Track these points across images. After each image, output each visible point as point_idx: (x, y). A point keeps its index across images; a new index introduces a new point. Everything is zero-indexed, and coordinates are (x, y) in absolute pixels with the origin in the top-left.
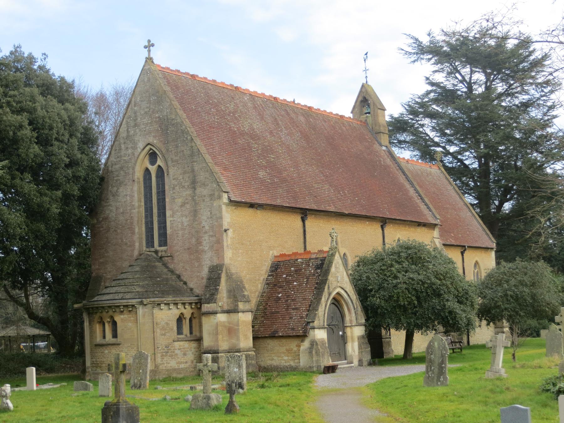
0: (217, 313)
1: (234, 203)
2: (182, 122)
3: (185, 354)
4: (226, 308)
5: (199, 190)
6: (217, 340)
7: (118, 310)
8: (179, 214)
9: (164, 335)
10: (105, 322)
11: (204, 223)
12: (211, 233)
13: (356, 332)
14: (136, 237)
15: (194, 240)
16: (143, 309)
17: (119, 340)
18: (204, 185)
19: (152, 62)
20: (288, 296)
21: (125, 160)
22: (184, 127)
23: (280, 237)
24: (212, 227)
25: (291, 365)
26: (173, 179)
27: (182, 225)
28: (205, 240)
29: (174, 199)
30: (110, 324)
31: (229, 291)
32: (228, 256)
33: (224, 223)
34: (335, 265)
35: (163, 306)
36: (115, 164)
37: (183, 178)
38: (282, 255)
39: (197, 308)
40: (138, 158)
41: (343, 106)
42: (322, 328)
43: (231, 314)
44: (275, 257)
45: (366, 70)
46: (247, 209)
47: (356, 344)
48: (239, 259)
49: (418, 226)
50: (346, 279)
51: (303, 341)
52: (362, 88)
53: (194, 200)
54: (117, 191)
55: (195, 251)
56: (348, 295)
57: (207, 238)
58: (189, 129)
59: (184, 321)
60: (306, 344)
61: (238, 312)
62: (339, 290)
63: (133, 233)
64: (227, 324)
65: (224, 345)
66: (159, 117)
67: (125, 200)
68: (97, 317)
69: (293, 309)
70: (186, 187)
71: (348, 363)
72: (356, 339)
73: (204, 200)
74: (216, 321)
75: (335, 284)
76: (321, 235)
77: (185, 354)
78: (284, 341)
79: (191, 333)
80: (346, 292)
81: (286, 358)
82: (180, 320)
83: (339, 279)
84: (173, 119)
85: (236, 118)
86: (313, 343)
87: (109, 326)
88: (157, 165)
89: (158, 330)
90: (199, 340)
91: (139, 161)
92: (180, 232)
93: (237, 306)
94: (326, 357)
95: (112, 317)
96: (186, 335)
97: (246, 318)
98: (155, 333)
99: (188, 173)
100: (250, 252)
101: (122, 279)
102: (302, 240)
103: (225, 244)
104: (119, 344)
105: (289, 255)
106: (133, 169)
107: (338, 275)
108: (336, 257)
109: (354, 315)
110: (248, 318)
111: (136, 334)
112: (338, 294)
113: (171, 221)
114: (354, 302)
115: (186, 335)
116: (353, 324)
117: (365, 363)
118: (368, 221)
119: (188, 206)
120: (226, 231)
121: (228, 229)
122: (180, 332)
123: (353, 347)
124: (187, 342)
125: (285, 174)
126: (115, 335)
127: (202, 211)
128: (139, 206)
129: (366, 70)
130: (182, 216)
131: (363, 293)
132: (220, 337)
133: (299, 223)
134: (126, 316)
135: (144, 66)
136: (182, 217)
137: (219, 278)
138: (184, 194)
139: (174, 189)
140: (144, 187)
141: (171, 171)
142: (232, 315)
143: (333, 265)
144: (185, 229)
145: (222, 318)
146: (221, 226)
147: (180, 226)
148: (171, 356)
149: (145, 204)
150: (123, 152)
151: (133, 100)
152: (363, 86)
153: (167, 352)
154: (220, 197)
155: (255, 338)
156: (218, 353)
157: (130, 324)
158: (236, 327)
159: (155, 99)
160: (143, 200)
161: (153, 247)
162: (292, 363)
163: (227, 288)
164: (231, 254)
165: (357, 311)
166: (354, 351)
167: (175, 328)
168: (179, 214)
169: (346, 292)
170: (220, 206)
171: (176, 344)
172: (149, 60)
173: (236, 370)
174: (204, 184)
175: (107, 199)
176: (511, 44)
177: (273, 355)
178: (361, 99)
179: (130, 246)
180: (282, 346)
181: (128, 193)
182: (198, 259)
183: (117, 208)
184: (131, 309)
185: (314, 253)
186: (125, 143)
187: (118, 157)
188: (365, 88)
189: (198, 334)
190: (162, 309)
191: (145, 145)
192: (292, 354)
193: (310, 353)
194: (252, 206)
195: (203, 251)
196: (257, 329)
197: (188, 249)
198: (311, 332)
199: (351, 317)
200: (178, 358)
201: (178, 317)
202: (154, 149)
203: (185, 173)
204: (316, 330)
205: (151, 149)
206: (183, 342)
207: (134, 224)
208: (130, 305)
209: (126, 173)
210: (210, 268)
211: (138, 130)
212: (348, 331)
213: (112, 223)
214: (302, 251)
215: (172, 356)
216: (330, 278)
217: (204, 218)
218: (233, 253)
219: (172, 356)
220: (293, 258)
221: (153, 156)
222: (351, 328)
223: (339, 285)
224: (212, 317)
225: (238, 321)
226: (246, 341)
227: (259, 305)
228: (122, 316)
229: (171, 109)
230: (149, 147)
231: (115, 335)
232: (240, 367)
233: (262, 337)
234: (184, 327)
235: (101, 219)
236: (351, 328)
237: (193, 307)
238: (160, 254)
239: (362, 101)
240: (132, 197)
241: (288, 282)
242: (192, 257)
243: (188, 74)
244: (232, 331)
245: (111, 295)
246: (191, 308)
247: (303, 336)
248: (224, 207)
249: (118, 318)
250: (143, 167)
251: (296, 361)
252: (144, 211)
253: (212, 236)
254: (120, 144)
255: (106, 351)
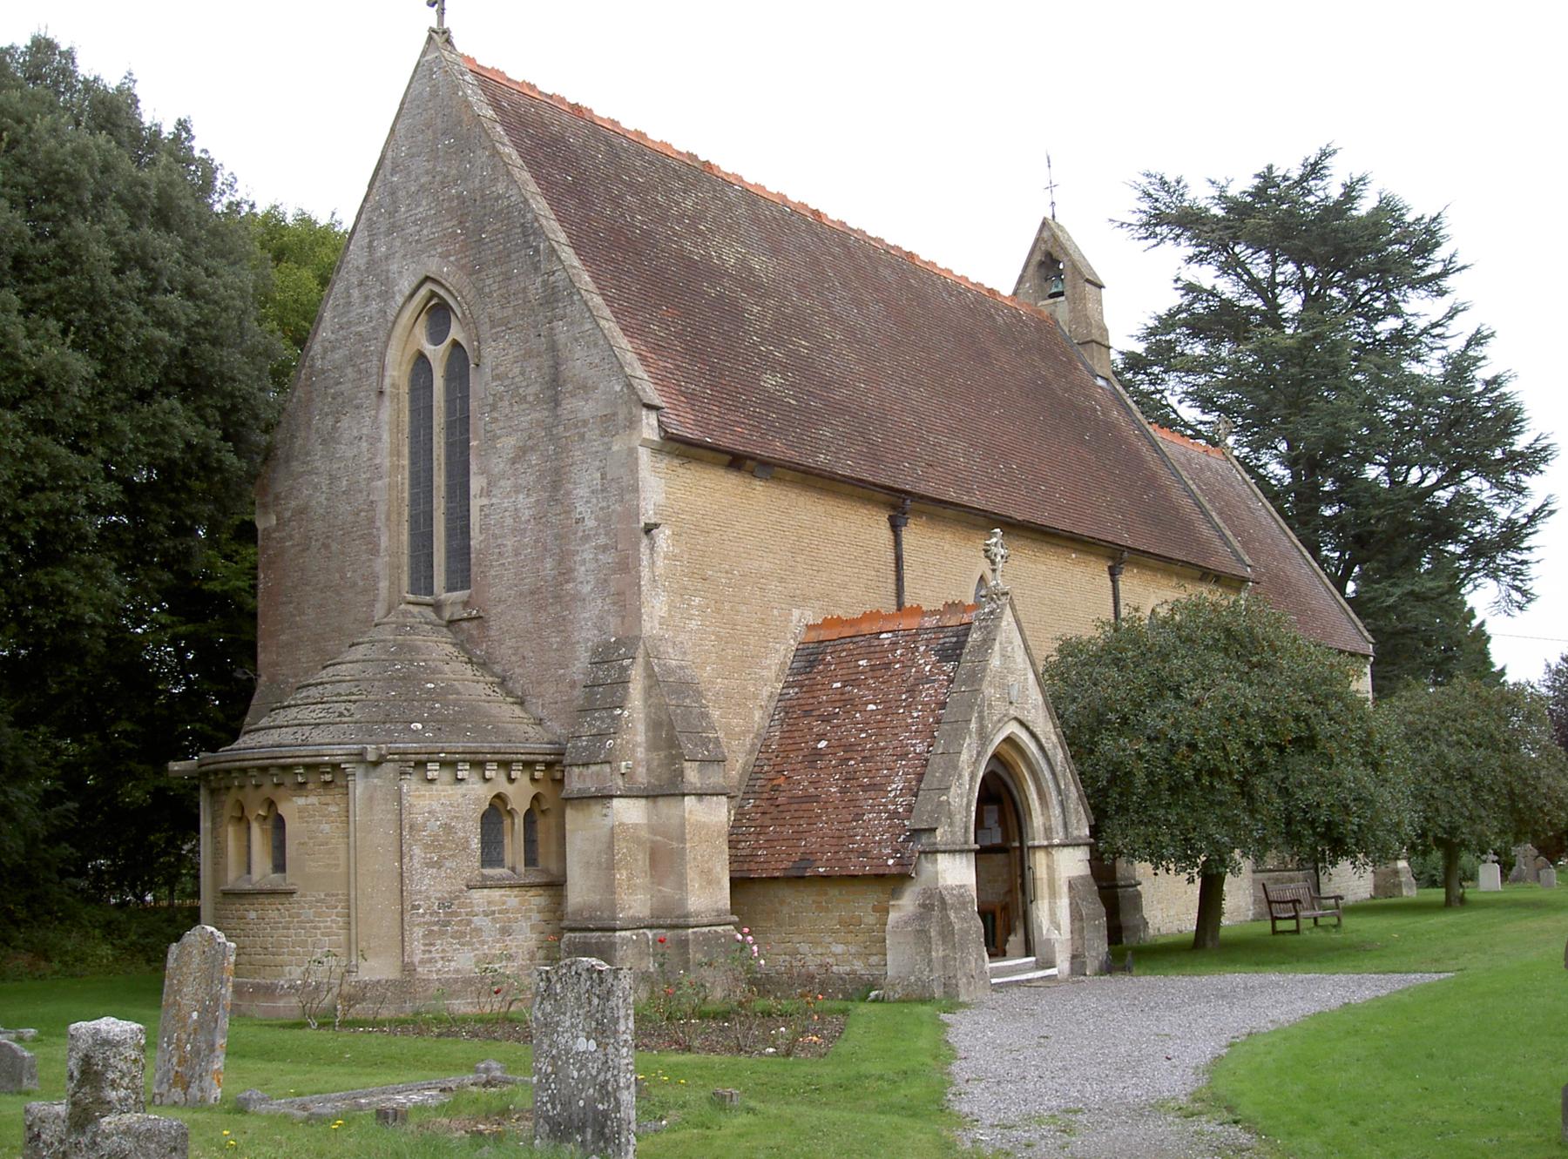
0: (612, 797)
1: (679, 447)
2: (526, 201)
3: (505, 931)
4: (642, 777)
5: (568, 405)
6: (610, 887)
7: (288, 780)
8: (507, 484)
9: (438, 865)
10: (252, 818)
11: (581, 508)
12: (602, 540)
13: (1061, 869)
14: (381, 564)
15: (549, 563)
16: (366, 775)
17: (290, 880)
18: (585, 388)
19: (448, 41)
20: (849, 748)
21: (359, 334)
22: (529, 216)
23: (828, 562)
24: (605, 520)
25: (853, 972)
26: (494, 379)
27: (516, 518)
28: (583, 562)
29: (495, 438)
30: (268, 826)
31: (655, 725)
32: (655, 610)
33: (642, 504)
34: (1003, 649)
35: (433, 770)
36: (334, 349)
37: (522, 374)
38: (828, 623)
39: (554, 780)
40: (394, 323)
41: (997, 268)
42: (961, 851)
43: (661, 802)
44: (809, 627)
45: (1051, 187)
46: (722, 472)
47: (1064, 903)
48: (693, 625)
49: (1201, 579)
50: (1035, 696)
51: (896, 893)
52: (1041, 231)
53: (554, 439)
54: (334, 428)
55: (554, 598)
56: (1041, 748)
57: (588, 556)
58: (544, 222)
59: (507, 822)
60: (907, 903)
61: (684, 795)
62: (1013, 728)
63: (374, 551)
64: (644, 834)
65: (636, 902)
66: (459, 196)
67: (355, 451)
68: (229, 800)
69: (865, 788)
70: (530, 399)
71: (1039, 966)
72: (1065, 889)
73: (582, 437)
74: (608, 822)
75: (999, 708)
76: (945, 568)
77: (505, 931)
78: (834, 892)
79: (530, 860)
80: (1033, 735)
81: (839, 949)
82: (495, 812)
83: (1014, 693)
84: (499, 197)
85: (700, 233)
86: (935, 903)
87: (263, 830)
88: (449, 340)
89: (417, 850)
90: (555, 885)
91: (399, 331)
92: (510, 543)
93: (681, 773)
94: (972, 948)
95: (271, 804)
96: (513, 869)
97: (710, 817)
98: (406, 860)
99: (539, 355)
100: (727, 606)
101: (316, 685)
102: (892, 587)
103: (645, 573)
104: (291, 893)
105: (852, 622)
106: (382, 356)
107: (1010, 679)
108: (1004, 624)
109: (1056, 811)
110: (714, 815)
111: (342, 861)
112: (1009, 740)
113: (482, 508)
114: (1058, 769)
115: (513, 869)
116: (1056, 841)
117: (1092, 965)
118: (1075, 550)
119: (534, 459)
120: (649, 529)
121: (656, 526)
122: (491, 852)
123: (1053, 913)
124: (516, 891)
125: (840, 394)
126: (280, 866)
127: (575, 469)
128: (396, 468)
129: (1051, 187)
130: (517, 489)
131: (1080, 739)
132: (621, 875)
133: (885, 534)
134: (313, 800)
135: (424, 54)
136: (517, 492)
137: (624, 682)
138: (525, 421)
139: (494, 407)
140: (412, 411)
141: (490, 352)
142: (662, 804)
143: (997, 647)
144: (525, 530)
145: (629, 812)
146: (634, 514)
147: (509, 521)
148: (459, 935)
149: (413, 463)
150: (356, 310)
151: (389, 154)
152: (1044, 223)
153: (447, 923)
154: (632, 424)
155: (737, 883)
156: (614, 930)
157: (326, 827)
158: (675, 845)
159: (450, 146)
160: (406, 451)
161: (431, 593)
162: (859, 966)
163: (648, 715)
164: (665, 608)
165: (1068, 797)
166: (1058, 928)
167: (475, 844)
168: (507, 484)
169: (1033, 735)
170: (632, 452)
171: (478, 896)
172: (440, 38)
173: (584, 1045)
174: (584, 387)
175: (308, 454)
176: (1364, 206)
177: (796, 938)
178: (1038, 257)
179: (365, 591)
180: (827, 910)
181: (365, 431)
182: (561, 624)
183: (333, 479)
184: (328, 778)
185: (933, 613)
186: (361, 284)
187: (341, 328)
188: (1051, 229)
189: (553, 866)
190: (432, 781)
191: (416, 282)
192: (861, 938)
193: (922, 935)
194: (736, 462)
195: (577, 598)
196: (748, 851)
197: (532, 593)
198: (926, 866)
199: (1048, 818)
200: (483, 943)
201: (486, 806)
202: (442, 292)
203: (529, 354)
204: (615, 802)
205: (433, 294)
206: (502, 892)
207: (378, 524)
208: (297, 765)
209: (360, 372)
210: (595, 653)
211: (398, 243)
212: (1040, 862)
213: (318, 524)
214: (890, 606)
215: (464, 934)
216: (989, 691)
217: (582, 491)
218: (672, 606)
219: (464, 934)
220: (866, 628)
221: (438, 314)
222: (1049, 854)
223: (1012, 712)
224: (597, 809)
225: (683, 825)
226: (707, 894)
227: (753, 774)
228: (301, 801)
229: (494, 167)
230: (429, 286)
231: (280, 866)
232: (603, 1030)
233: (761, 879)
234: (507, 840)
235: (288, 514)
236: (1049, 854)
237: (538, 775)
238: (447, 615)
239: (1041, 264)
240: (374, 440)
241: (848, 703)
242: (542, 617)
243: (562, 100)
244: (664, 857)
245: (275, 732)
246: (533, 780)
247: (894, 881)
248: (644, 455)
249: (291, 808)
250: (411, 351)
251: (874, 960)
252: (407, 482)
253: (605, 548)
254: (347, 289)
255: (253, 915)
